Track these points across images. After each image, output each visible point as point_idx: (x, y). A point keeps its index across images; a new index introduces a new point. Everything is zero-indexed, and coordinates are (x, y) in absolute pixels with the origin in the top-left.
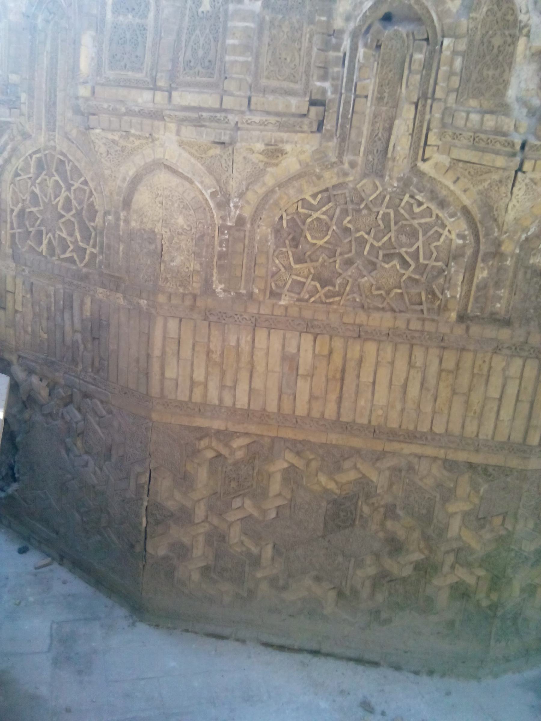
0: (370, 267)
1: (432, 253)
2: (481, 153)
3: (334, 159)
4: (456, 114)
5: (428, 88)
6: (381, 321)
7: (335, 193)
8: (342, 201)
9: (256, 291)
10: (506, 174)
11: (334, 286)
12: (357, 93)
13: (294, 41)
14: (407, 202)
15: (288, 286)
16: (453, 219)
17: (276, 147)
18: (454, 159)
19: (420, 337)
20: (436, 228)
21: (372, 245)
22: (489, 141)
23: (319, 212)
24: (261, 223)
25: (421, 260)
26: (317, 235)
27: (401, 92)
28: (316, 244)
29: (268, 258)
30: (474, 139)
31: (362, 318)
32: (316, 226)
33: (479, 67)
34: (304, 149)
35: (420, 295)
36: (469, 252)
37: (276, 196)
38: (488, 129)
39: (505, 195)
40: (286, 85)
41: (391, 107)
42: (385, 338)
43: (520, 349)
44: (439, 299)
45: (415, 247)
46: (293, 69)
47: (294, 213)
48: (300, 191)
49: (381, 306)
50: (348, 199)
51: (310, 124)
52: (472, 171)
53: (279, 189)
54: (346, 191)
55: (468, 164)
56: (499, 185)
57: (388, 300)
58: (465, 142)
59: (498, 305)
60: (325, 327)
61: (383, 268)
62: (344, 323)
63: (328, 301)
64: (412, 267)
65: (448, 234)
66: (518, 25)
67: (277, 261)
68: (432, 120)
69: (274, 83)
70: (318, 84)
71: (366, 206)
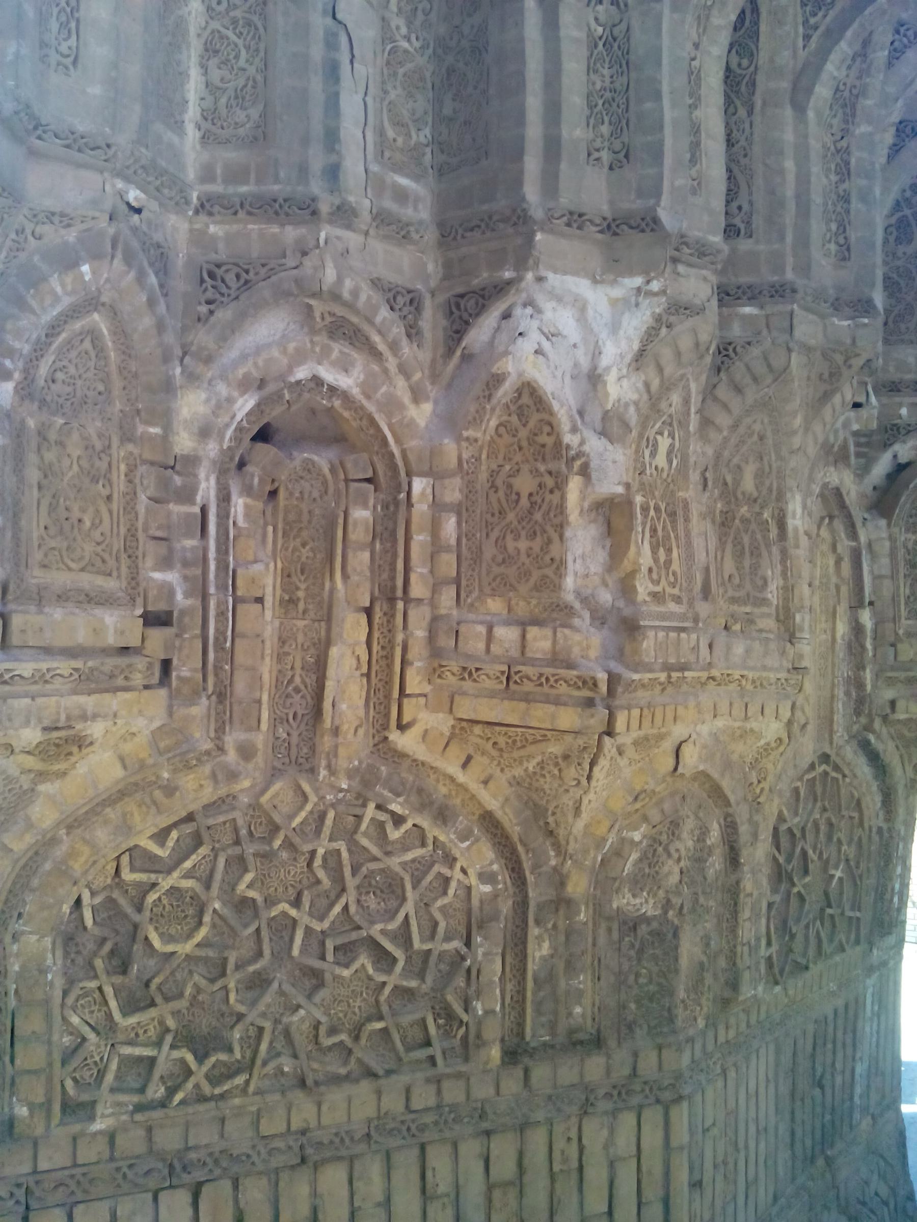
0: (308, 983)
1: (436, 924)
2: (523, 705)
3: (208, 745)
4: (463, 629)
5: (393, 578)
6: (349, 1107)
7: (211, 822)
8: (227, 839)
9: (22, 1111)
10: (581, 741)
11: (230, 1050)
12: (239, 593)
13: (95, 480)
14: (372, 819)
15: (110, 1078)
16: (467, 843)
17: (71, 732)
18: (461, 720)
19: (436, 1123)
20: (437, 868)
21: (308, 930)
22: (543, 680)
23: (176, 874)
24: (19, 926)
25: (417, 944)
26: (172, 931)
27: (333, 590)
28: (173, 953)
29: (48, 1017)
30: (508, 679)
31: (304, 1112)
32: (168, 907)
33: (494, 535)
34: (134, 730)
35: (423, 1022)
36: (506, 907)
37: (60, 852)
38: (538, 656)
39: (574, 783)
40: (87, 581)
41: (314, 621)
42: (361, 1148)
43: (627, 1093)
44: (461, 1022)
45: (401, 916)
46: (98, 544)
47: (110, 886)
48: (125, 828)
49: (343, 1071)
50: (243, 832)
51: (148, 668)
52: (502, 741)
53: (68, 834)
54: (237, 814)
55: (497, 728)
56: (563, 764)
57: (358, 1053)
58: (488, 684)
59: (578, 1010)
60: (216, 1162)
61: (336, 978)
62: (264, 1137)
63: (217, 1091)
64: (401, 964)
65: (461, 876)
66: (564, 452)
67: (75, 1020)
68: (410, 643)
69: (60, 579)
70: (157, 576)
71: (288, 844)
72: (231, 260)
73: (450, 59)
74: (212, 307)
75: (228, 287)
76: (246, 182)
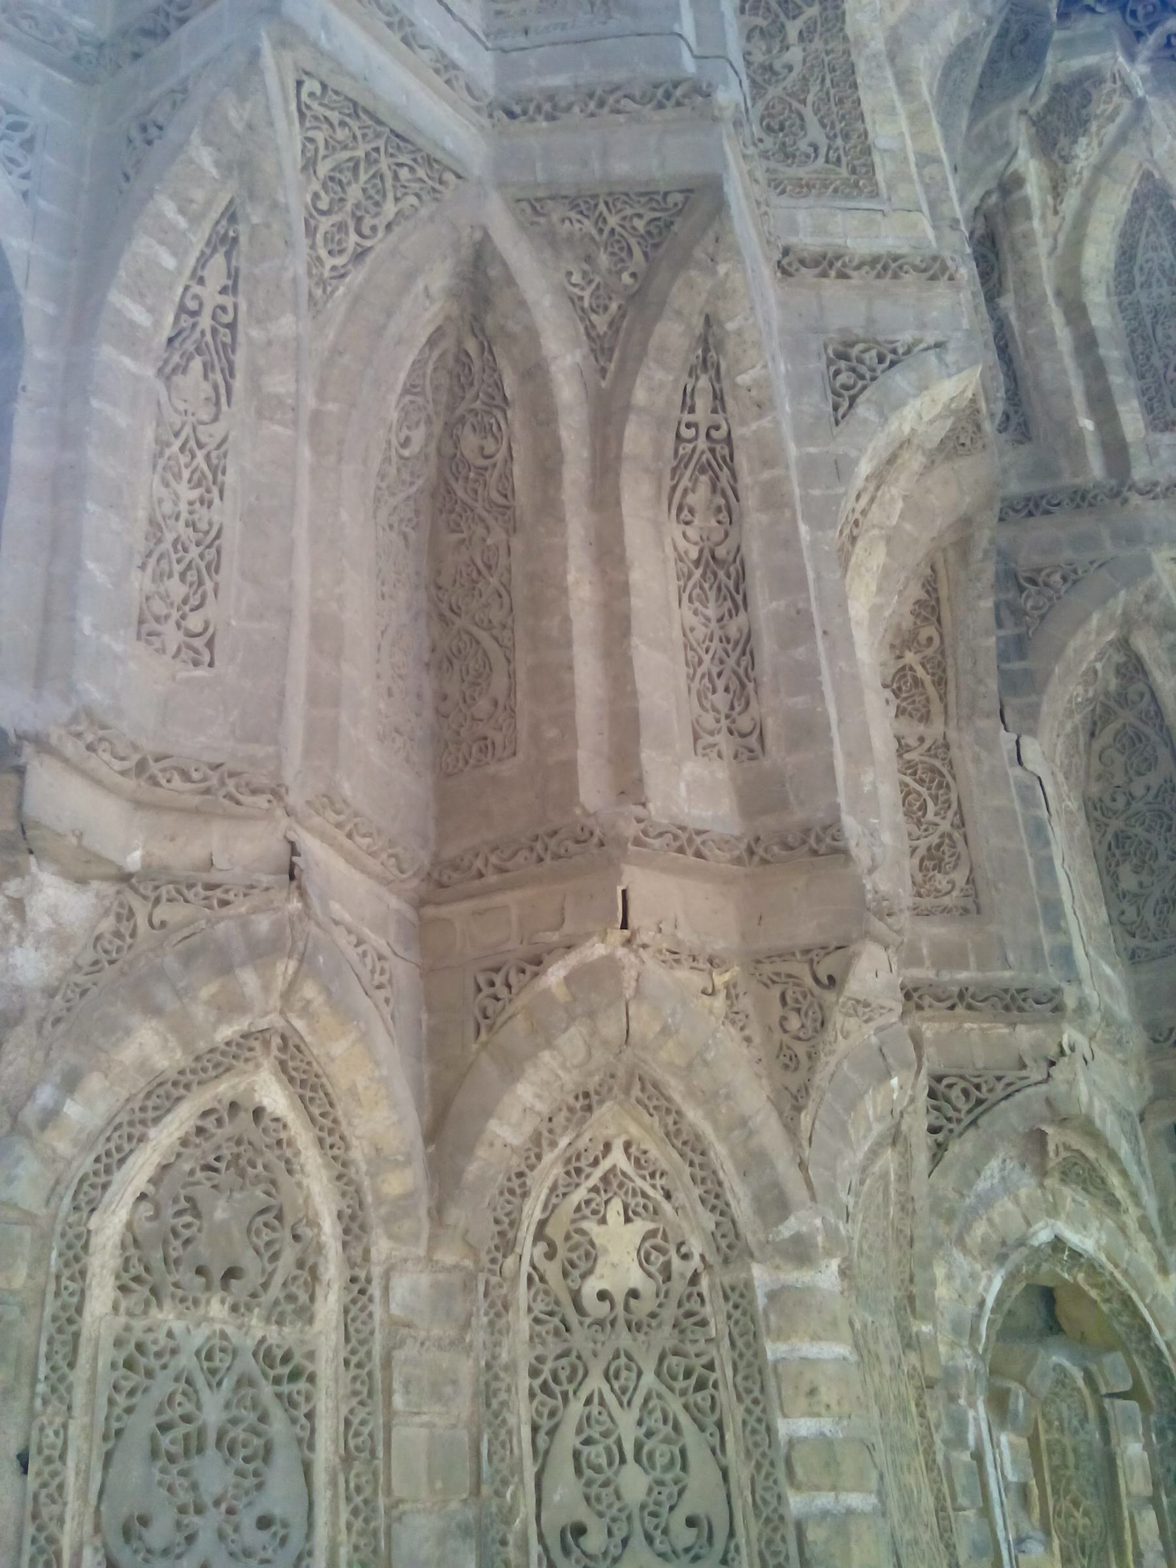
72: (954, 1071)
73: (1116, 824)
74: (940, 1137)
75: (956, 1109)
76: (966, 967)
